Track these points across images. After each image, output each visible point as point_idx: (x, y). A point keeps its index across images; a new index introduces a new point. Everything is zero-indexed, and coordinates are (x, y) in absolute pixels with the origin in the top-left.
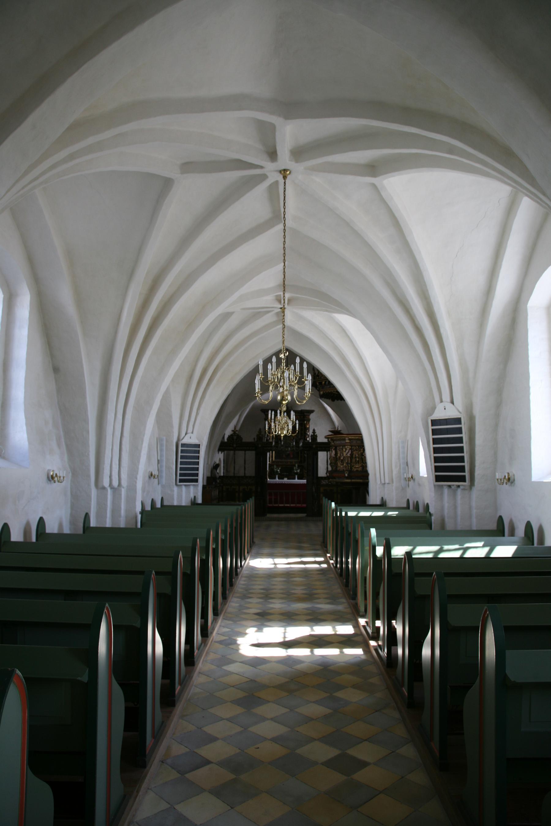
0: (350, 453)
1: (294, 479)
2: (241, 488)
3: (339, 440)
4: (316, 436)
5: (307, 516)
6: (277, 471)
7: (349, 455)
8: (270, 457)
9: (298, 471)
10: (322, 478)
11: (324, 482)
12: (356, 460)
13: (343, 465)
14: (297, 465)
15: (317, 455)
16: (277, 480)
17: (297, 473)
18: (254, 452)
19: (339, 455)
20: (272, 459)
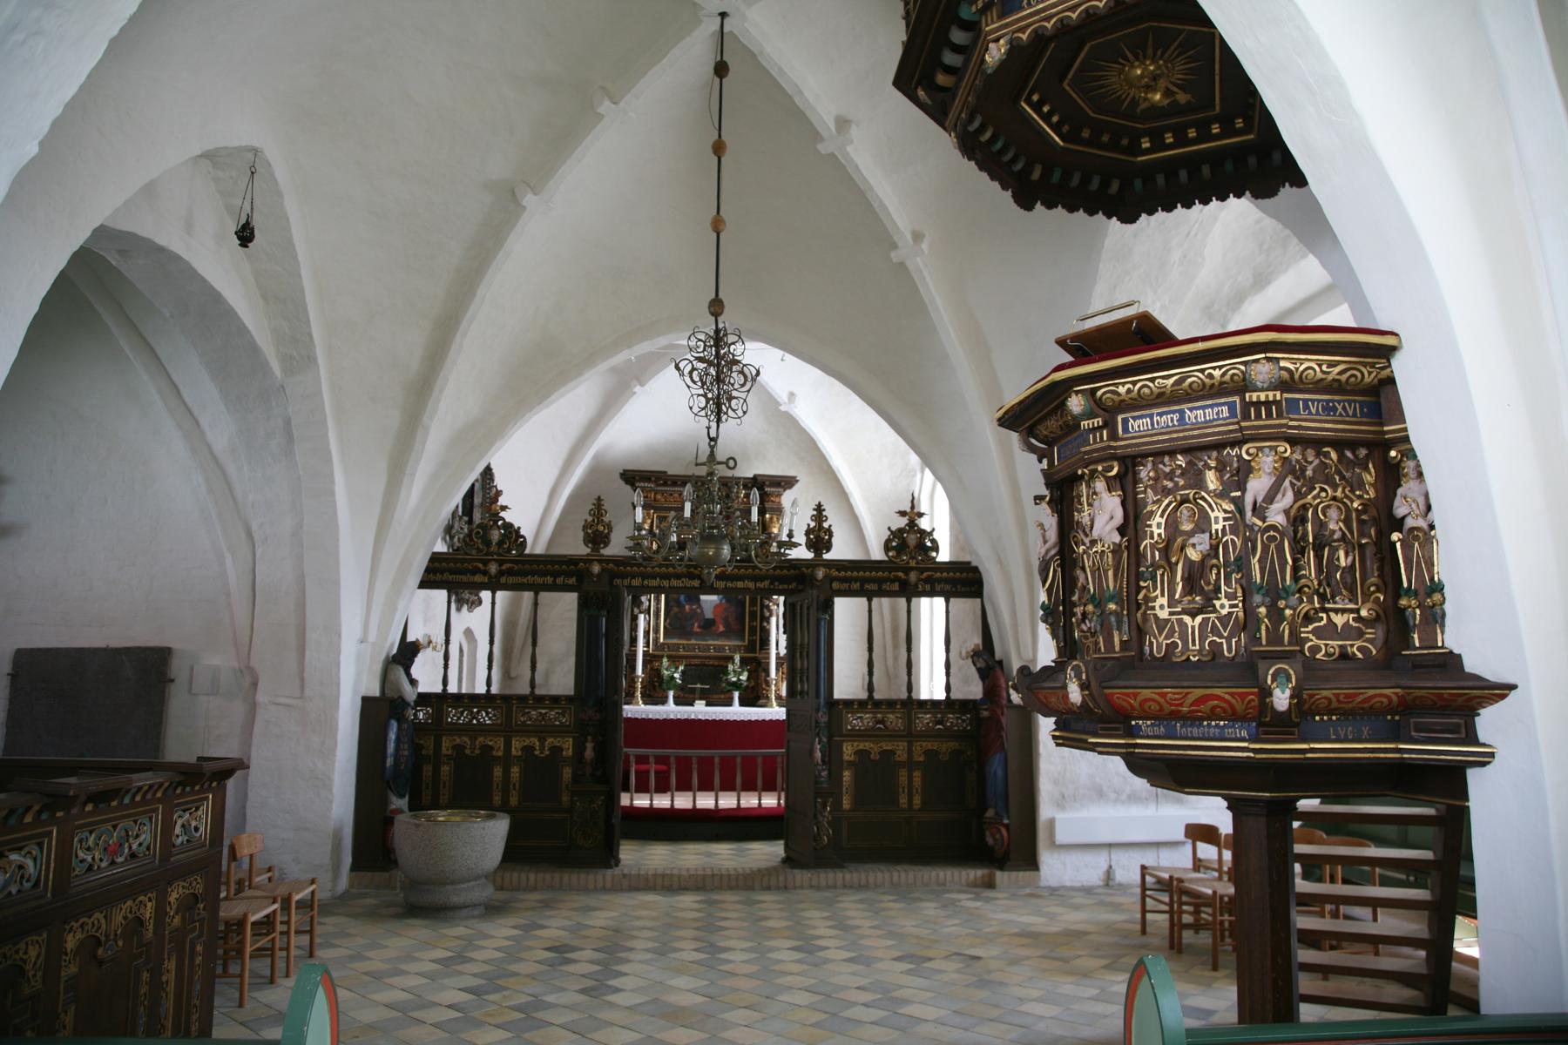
0: (1286, 499)
1: (729, 703)
2: (517, 745)
3: (1163, 399)
4: (829, 532)
5: (790, 861)
6: (672, 678)
7: (1276, 517)
8: (647, 626)
9: (744, 677)
10: (847, 703)
11: (855, 721)
12: (1326, 569)
13: (1207, 606)
14: (737, 658)
15: (828, 607)
16: (671, 710)
17: (736, 685)
18: (574, 596)
19: (1157, 526)
20: (656, 639)
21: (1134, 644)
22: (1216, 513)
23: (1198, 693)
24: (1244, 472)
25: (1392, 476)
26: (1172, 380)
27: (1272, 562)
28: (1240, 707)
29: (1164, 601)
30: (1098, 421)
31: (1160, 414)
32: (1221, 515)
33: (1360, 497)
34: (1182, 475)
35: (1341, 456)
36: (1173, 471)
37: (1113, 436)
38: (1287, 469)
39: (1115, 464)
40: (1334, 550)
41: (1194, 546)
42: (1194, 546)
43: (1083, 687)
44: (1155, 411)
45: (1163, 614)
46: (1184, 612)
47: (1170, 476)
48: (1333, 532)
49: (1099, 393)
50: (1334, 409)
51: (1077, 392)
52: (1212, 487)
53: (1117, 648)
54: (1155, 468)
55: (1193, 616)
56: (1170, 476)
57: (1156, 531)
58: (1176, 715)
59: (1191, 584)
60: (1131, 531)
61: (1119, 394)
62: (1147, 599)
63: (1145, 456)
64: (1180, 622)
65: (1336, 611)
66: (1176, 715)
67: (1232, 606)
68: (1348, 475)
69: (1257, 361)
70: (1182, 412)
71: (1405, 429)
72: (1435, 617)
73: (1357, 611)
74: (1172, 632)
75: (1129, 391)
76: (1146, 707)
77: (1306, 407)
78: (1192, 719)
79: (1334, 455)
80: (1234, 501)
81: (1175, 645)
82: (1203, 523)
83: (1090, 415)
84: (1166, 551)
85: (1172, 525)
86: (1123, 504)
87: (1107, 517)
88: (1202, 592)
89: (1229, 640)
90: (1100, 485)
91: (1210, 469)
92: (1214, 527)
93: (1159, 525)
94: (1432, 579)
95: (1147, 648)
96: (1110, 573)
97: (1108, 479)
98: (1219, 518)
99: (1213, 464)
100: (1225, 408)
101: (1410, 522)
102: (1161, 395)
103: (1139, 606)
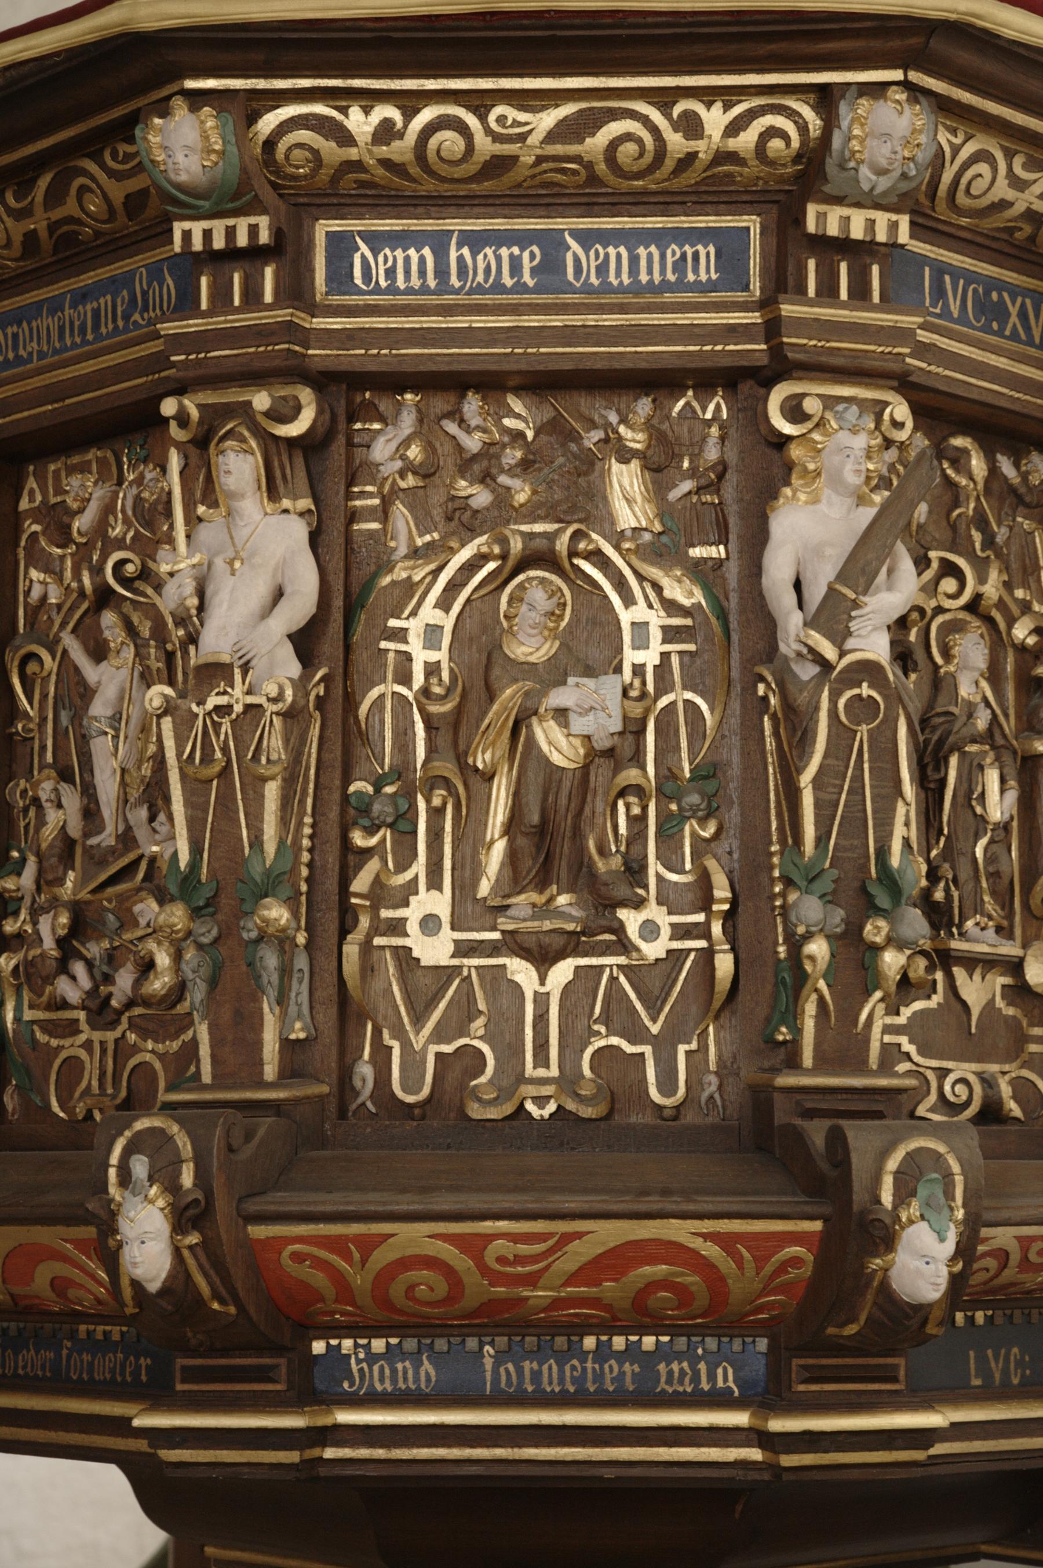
3: (497, 187)
19: (423, 637)
21: (326, 1055)
22: (640, 612)
23: (609, 1234)
24: (770, 467)
26: (548, 119)
27: (857, 789)
28: (742, 1281)
30: (254, 227)
31: (475, 241)
32: (656, 619)
34: (526, 466)
35: (993, 470)
36: (490, 452)
37: (296, 291)
39: (306, 395)
40: (972, 770)
41: (561, 715)
42: (561, 715)
43: (185, 1216)
44: (456, 225)
45: (434, 950)
47: (482, 466)
49: (269, 122)
50: (1001, 313)
51: (197, 99)
52: (626, 518)
53: (270, 1072)
54: (427, 427)
55: (543, 958)
56: (482, 466)
58: (504, 1320)
59: (548, 844)
60: (330, 645)
61: (346, 138)
62: (380, 894)
63: (395, 382)
64: (496, 977)
65: (971, 962)
66: (504, 1320)
67: (680, 932)
68: (1001, 534)
69: (877, 90)
70: (552, 246)
74: (464, 1013)
75: (386, 132)
76: (397, 1291)
78: (551, 1329)
79: (978, 464)
80: (703, 573)
82: (589, 646)
83: (228, 198)
84: (452, 732)
86: (315, 540)
87: (260, 590)
88: (583, 878)
89: (665, 1047)
90: (239, 467)
91: (625, 456)
92: (631, 656)
93: (432, 633)
95: (365, 1071)
96: (272, 791)
97: (270, 443)
98: (645, 627)
99: (634, 439)
100: (707, 251)
102: (499, 165)
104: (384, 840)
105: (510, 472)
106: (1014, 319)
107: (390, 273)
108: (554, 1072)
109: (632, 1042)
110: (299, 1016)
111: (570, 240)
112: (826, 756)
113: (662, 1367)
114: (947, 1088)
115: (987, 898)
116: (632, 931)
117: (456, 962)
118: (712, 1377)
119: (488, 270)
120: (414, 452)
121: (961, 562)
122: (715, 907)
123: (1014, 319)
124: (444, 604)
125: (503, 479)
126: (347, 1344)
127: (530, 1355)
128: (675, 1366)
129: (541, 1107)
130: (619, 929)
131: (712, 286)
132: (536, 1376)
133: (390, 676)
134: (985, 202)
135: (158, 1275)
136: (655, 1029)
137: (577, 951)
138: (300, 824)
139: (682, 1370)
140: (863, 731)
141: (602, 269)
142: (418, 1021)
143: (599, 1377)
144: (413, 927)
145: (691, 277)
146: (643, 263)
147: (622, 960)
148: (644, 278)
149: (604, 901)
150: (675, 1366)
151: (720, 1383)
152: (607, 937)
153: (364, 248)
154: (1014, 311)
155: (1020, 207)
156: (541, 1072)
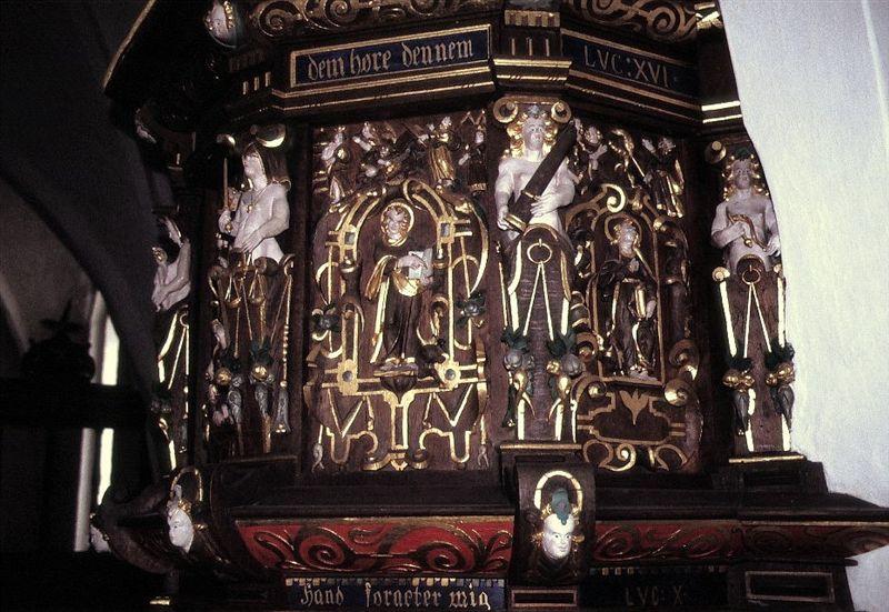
7: (545, 213)
19: (347, 232)
24: (499, 142)
25: (707, 188)
27: (540, 294)
29: (351, 365)
33: (663, 213)
35: (639, 147)
38: (565, 146)
40: (628, 292)
43: (196, 515)
45: (350, 388)
46: (385, 384)
48: (627, 260)
57: (343, 247)
65: (631, 388)
67: (465, 374)
68: (647, 179)
71: (737, 110)
72: (778, 403)
73: (660, 391)
77: (593, 57)
79: (629, 146)
80: (475, 199)
81: (366, 441)
85: (373, 243)
89: (459, 432)
94: (775, 341)
101: (740, 252)
103: (306, 374)
104: (328, 336)
105: (386, 159)
106: (640, 71)
107: (324, 71)
108: (406, 446)
109: (444, 431)
110: (282, 422)
111: (405, 47)
112: (522, 277)
113: (452, 594)
114: (618, 453)
115: (640, 356)
116: (442, 374)
117: (360, 393)
118: (477, 600)
119: (367, 64)
120: (341, 154)
121: (618, 189)
122: (479, 360)
123: (640, 71)
124: (354, 222)
125: (381, 162)
126: (302, 581)
127: (388, 588)
128: (458, 594)
129: (400, 464)
130: (434, 373)
131: (470, 59)
132: (391, 598)
133: (330, 258)
134: (610, 11)
135: (187, 542)
136: (454, 423)
137: (416, 385)
138: (282, 329)
139: (462, 596)
140: (541, 265)
141: (419, 57)
142: (342, 423)
143: (421, 599)
144: (339, 378)
145: (460, 56)
146: (438, 53)
147: (437, 390)
148: (438, 59)
149: (429, 358)
150: (458, 594)
151: (481, 603)
152: (429, 378)
153: (313, 62)
154: (640, 68)
155: (631, 14)
156: (399, 447)
